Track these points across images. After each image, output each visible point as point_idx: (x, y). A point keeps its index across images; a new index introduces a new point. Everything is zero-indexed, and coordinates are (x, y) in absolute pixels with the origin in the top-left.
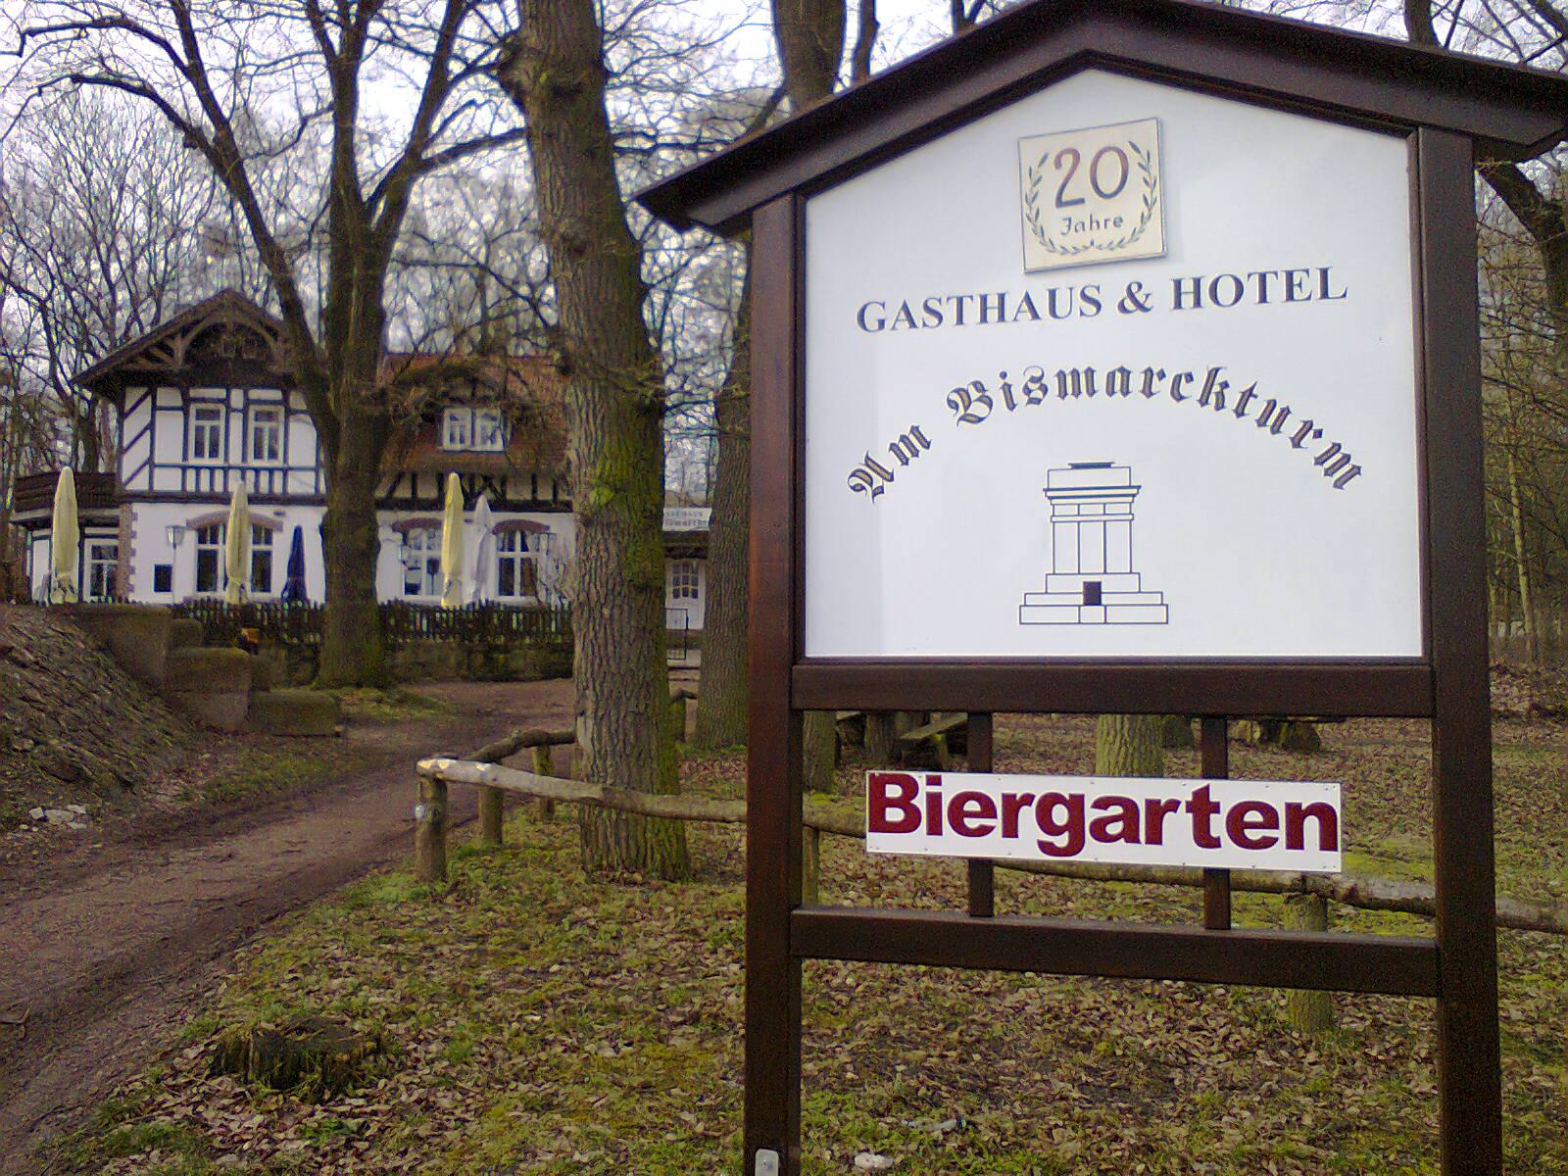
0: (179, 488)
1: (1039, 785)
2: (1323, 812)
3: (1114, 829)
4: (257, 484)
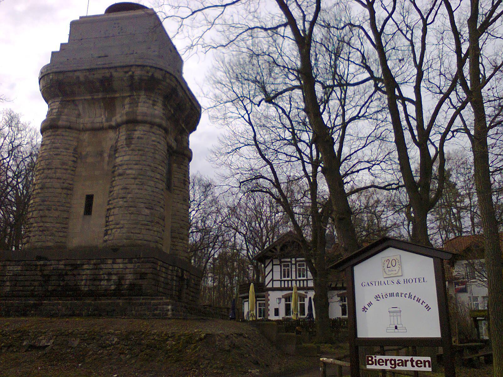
0: (280, 286)
1: (389, 357)
2: (428, 361)
3: (400, 364)
4: (300, 285)
